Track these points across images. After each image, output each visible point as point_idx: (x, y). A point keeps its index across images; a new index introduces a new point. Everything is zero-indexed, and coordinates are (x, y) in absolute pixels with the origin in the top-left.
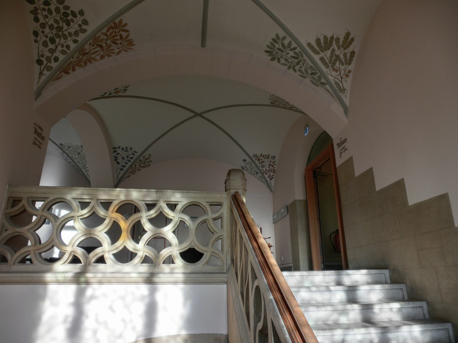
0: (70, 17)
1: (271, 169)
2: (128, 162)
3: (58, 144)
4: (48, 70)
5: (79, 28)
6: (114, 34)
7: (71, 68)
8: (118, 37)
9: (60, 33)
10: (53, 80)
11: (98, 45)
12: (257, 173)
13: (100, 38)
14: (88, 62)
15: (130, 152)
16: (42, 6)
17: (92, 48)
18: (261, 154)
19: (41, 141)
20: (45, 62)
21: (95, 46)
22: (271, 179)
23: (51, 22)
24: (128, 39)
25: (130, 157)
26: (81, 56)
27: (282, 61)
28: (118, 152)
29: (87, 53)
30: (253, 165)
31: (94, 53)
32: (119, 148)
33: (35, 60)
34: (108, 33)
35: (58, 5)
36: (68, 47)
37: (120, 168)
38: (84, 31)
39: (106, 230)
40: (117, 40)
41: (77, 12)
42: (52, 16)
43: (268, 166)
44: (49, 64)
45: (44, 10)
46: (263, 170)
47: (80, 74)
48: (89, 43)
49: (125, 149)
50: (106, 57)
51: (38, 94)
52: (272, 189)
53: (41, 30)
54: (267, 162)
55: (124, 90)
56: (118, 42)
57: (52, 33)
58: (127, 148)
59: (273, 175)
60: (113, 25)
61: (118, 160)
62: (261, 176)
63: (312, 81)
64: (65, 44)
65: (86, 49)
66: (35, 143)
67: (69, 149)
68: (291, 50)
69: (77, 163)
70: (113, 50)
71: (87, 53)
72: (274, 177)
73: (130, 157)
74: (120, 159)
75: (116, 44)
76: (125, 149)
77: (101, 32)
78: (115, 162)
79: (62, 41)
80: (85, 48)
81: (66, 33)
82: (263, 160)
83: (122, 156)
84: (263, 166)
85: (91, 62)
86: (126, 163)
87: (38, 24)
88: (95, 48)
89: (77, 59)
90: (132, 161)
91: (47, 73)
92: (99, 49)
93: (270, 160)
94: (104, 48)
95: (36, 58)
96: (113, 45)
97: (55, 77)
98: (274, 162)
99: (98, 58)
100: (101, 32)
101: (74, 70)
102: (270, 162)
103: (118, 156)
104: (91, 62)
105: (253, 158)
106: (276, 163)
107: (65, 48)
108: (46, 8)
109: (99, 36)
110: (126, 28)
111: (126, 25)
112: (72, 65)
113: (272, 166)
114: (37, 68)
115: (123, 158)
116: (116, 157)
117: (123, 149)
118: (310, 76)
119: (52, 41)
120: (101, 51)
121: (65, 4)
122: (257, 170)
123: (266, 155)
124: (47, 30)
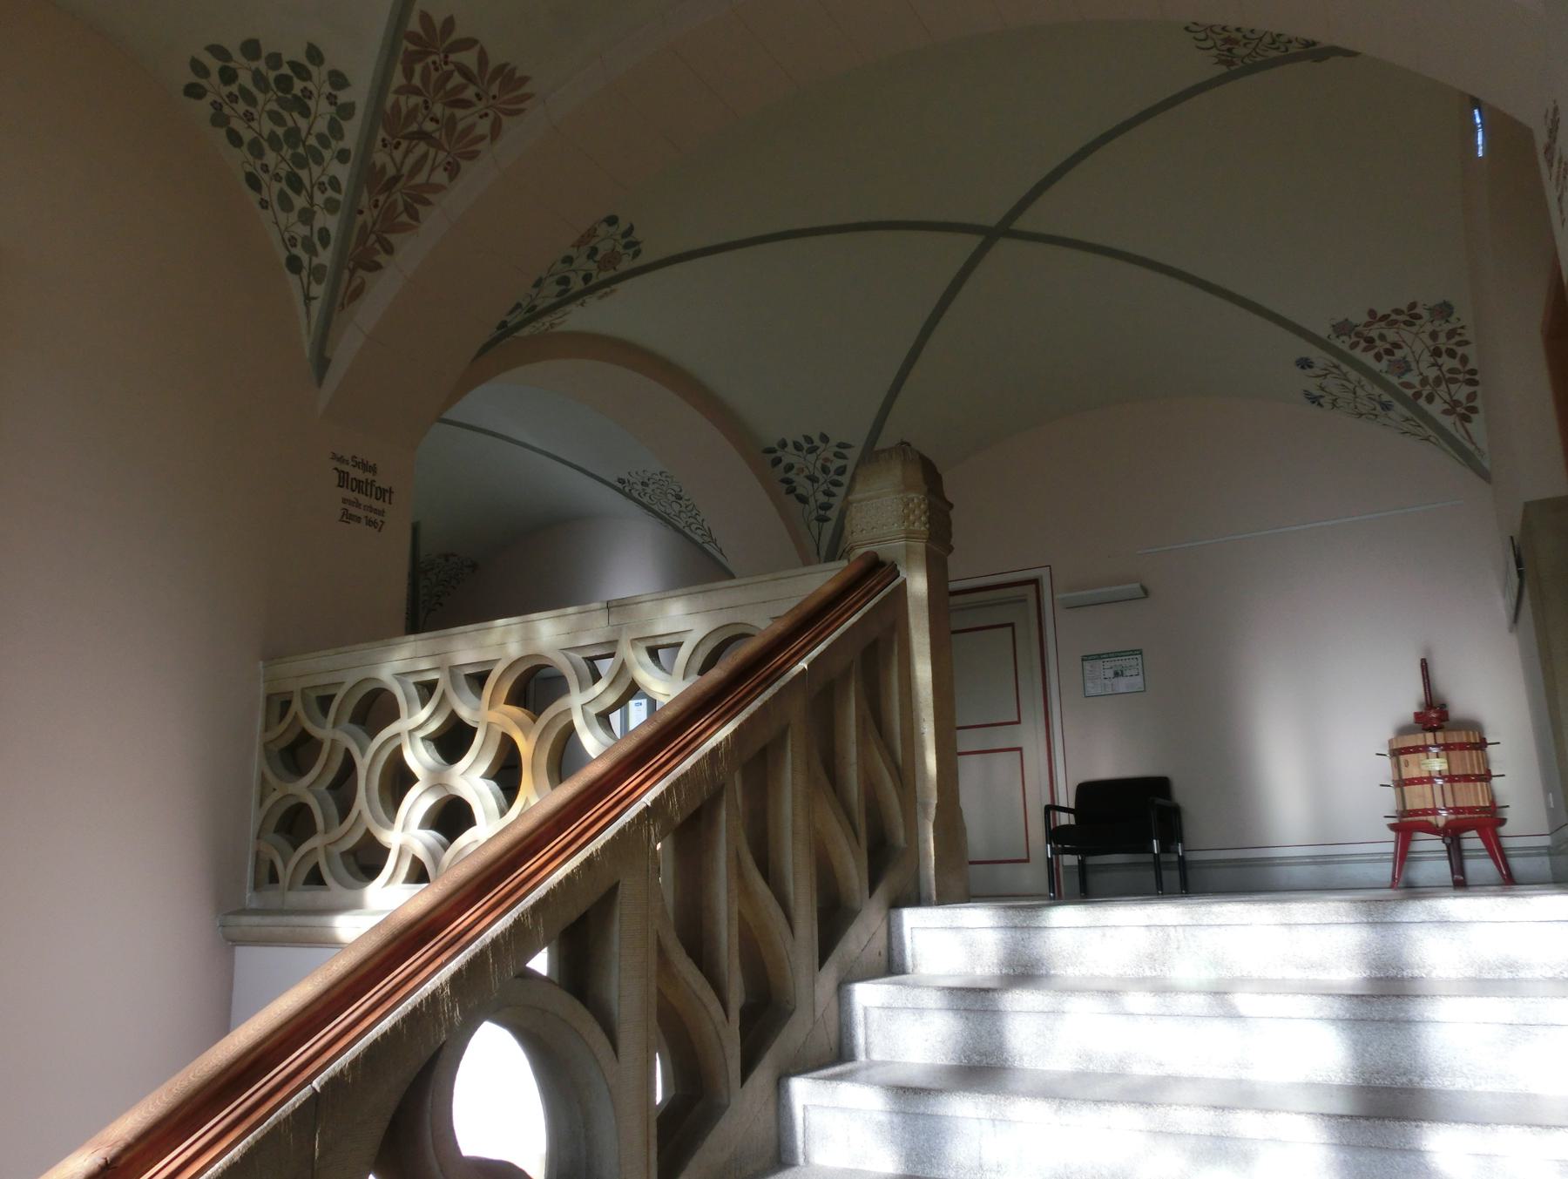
0: (298, 85)
1: (1451, 371)
2: (834, 489)
3: (613, 480)
4: (319, 282)
5: (333, 109)
6: (435, 75)
7: (377, 246)
8: (457, 79)
9: (301, 150)
10: (343, 306)
11: (411, 137)
12: (1386, 407)
13: (404, 111)
14: (418, 206)
15: (828, 452)
16: (225, 90)
17: (398, 154)
18: (1372, 313)
19: (378, 505)
20: (305, 257)
22: (1465, 419)
23: (267, 126)
24: (490, 69)
25: (833, 467)
26: (382, 198)
28: (787, 460)
29: (395, 179)
30: (1354, 375)
31: (417, 167)
32: (783, 444)
33: (283, 261)
34: (416, 81)
35: (254, 65)
36: (335, 183)
37: (814, 515)
38: (347, 111)
39: (484, 767)
40: (463, 88)
41: (302, 58)
42: (259, 107)
43: (1426, 358)
44: (315, 261)
45: (233, 98)
46: (1408, 385)
47: (411, 252)
48: (379, 143)
49: (806, 446)
50: (464, 164)
51: (322, 364)
52: (1487, 464)
53: (258, 163)
54: (1415, 344)
55: (626, 246)
56: (470, 93)
57: (283, 159)
58: (808, 439)
59: (1472, 397)
60: (412, 47)
61: (800, 491)
62: (1408, 414)
64: (325, 179)
65: (383, 168)
66: (347, 517)
67: (649, 490)
69: (687, 530)
70: (471, 127)
71: (395, 179)
72: (1478, 403)
73: (833, 467)
74: (804, 487)
75: (466, 104)
76: (806, 446)
77: (393, 88)
78: (792, 497)
79: (316, 170)
80: (378, 165)
81: (312, 141)
82: (1391, 335)
83: (806, 472)
84: (1403, 367)
85: (427, 203)
86: (828, 494)
87: (245, 148)
88: (408, 152)
89: (376, 212)
90: (845, 479)
91: (318, 290)
92: (422, 147)
93: (1429, 328)
94: (437, 135)
95: (283, 255)
96: (459, 113)
97: (345, 297)
98: (1451, 334)
99: (440, 177)
100: (393, 88)
101: (389, 249)
102: (1434, 335)
103: (791, 475)
104: (427, 203)
105: (1338, 343)
106: (1468, 335)
107: (330, 193)
108: (234, 88)
109: (396, 106)
110: (459, 33)
111: (449, 23)
112: (373, 237)
113: (1452, 354)
114: (293, 279)
115: (813, 479)
116: (788, 481)
117: (798, 447)
119: (296, 183)
120: (432, 151)
121: (264, 53)
122: (1377, 391)
123: (1398, 312)
124: (271, 158)
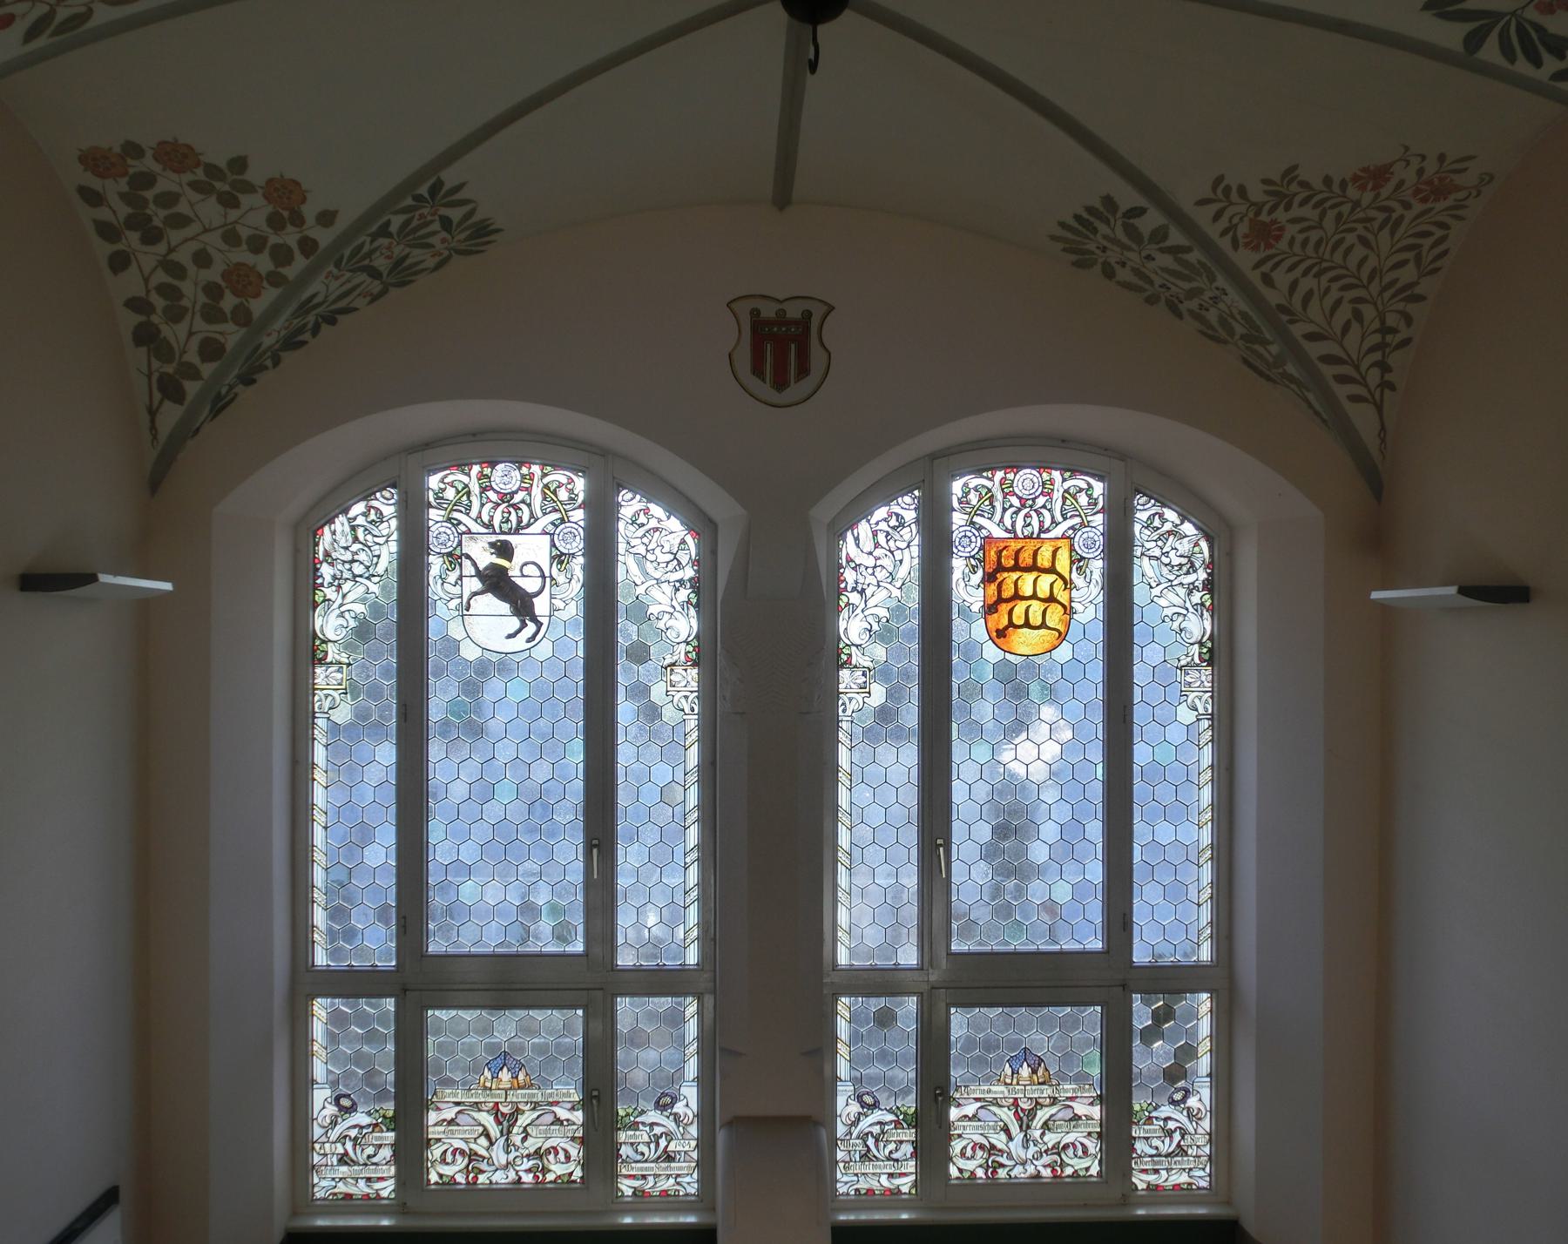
8: (436, 226)
21: (348, 275)
27: (1124, 274)
63: (1245, 361)
68: (1162, 250)
118: (1241, 343)
